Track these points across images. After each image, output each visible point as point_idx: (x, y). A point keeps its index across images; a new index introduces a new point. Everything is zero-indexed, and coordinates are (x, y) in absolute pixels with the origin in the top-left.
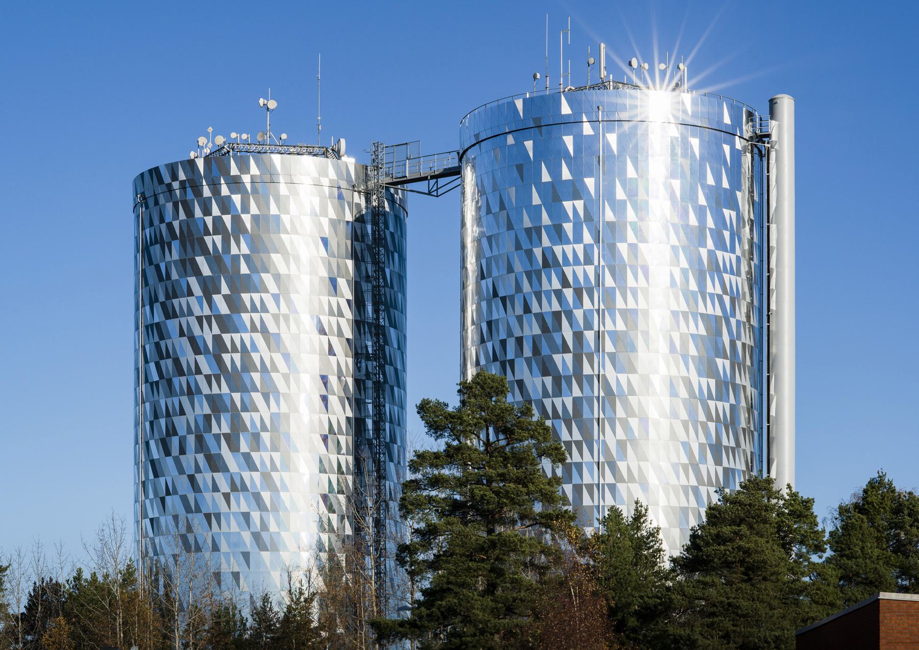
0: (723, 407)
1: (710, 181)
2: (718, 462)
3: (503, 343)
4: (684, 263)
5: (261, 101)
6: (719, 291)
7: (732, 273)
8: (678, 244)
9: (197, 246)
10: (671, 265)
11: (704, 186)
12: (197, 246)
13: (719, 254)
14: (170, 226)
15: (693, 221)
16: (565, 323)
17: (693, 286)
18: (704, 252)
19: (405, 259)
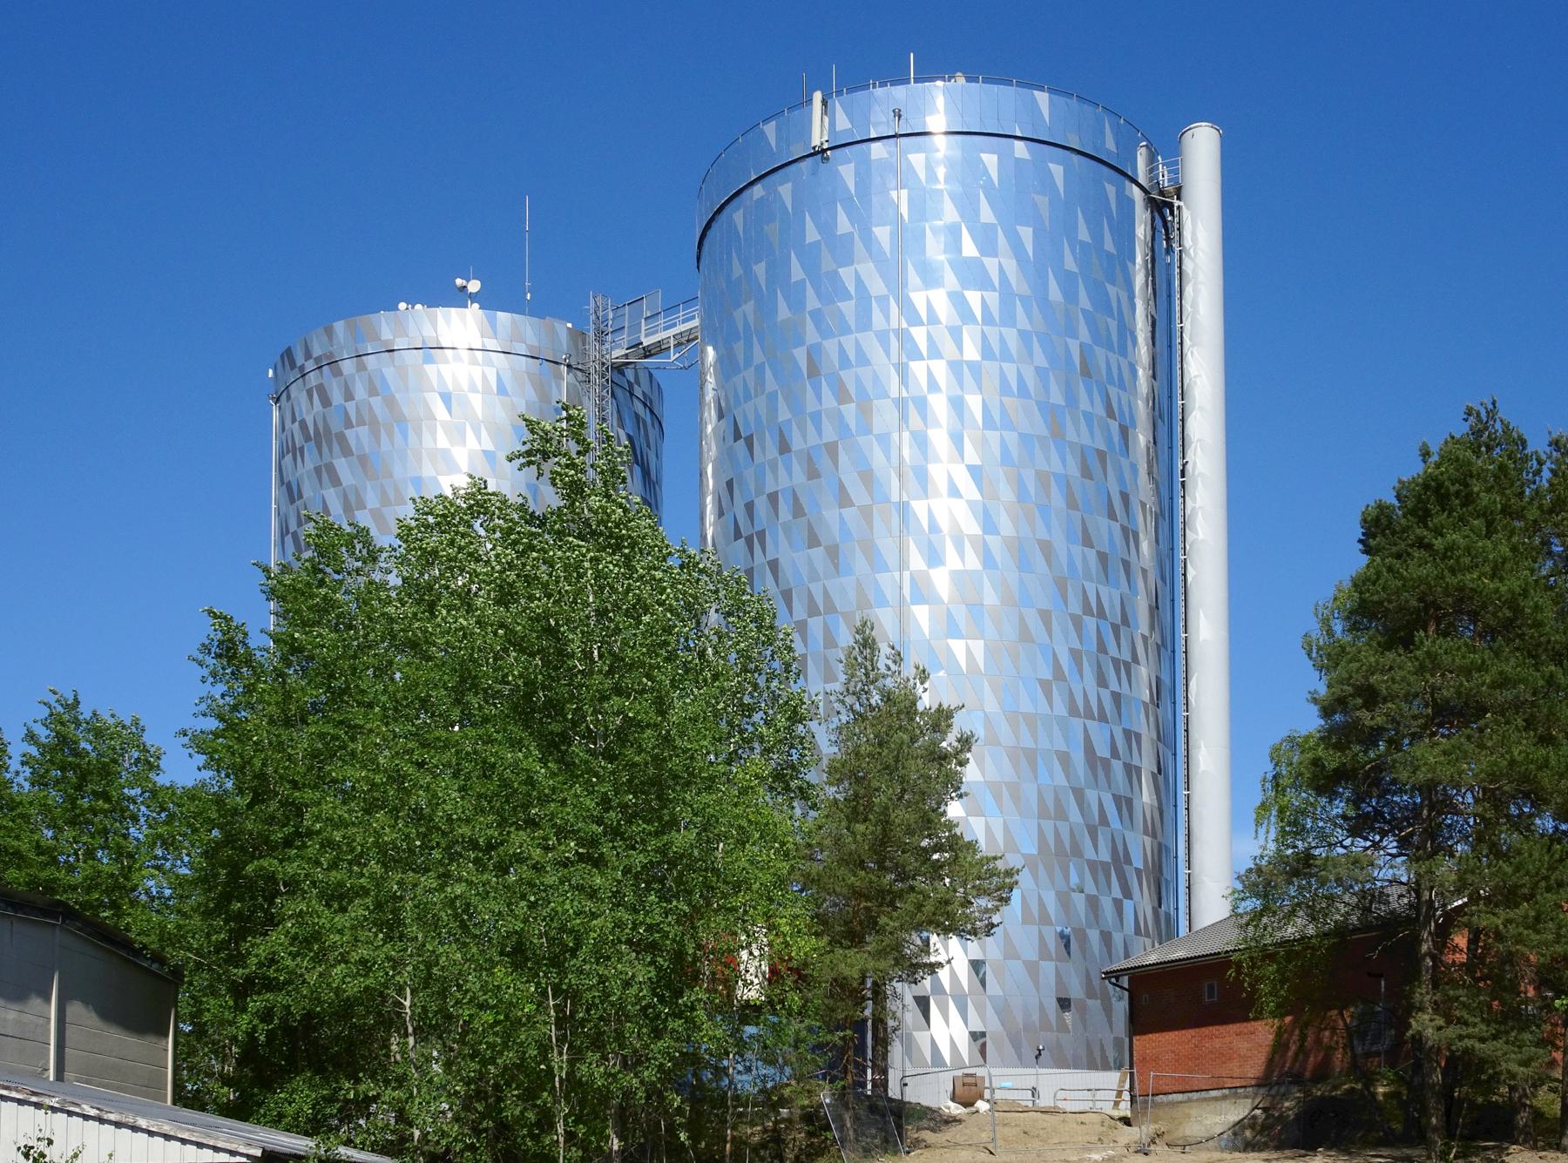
0: (1110, 597)
1: (1084, 234)
2: (1102, 682)
3: (750, 507)
4: (1040, 360)
5: (459, 282)
6: (1100, 410)
7: (1110, 347)
8: (1029, 328)
9: (336, 448)
10: (1099, 582)
11: (1073, 241)
12: (336, 448)
13: (1100, 353)
14: (303, 425)
15: (1055, 293)
16: (843, 458)
17: (1057, 397)
18: (1074, 347)
19: (658, 482)
